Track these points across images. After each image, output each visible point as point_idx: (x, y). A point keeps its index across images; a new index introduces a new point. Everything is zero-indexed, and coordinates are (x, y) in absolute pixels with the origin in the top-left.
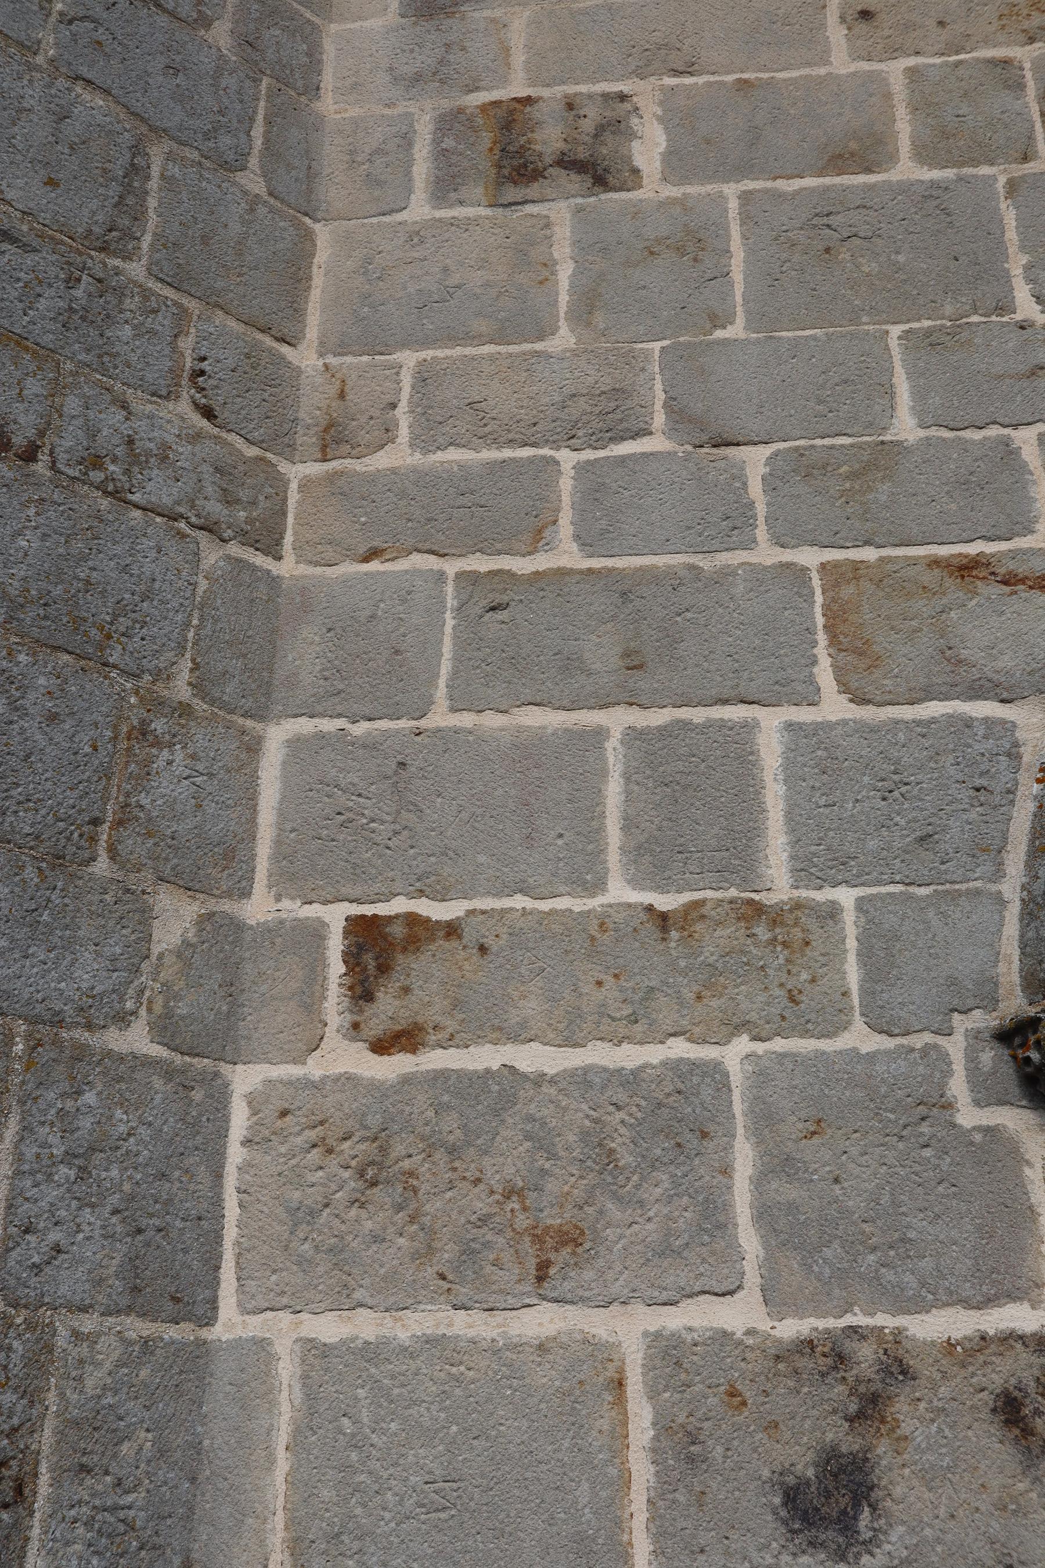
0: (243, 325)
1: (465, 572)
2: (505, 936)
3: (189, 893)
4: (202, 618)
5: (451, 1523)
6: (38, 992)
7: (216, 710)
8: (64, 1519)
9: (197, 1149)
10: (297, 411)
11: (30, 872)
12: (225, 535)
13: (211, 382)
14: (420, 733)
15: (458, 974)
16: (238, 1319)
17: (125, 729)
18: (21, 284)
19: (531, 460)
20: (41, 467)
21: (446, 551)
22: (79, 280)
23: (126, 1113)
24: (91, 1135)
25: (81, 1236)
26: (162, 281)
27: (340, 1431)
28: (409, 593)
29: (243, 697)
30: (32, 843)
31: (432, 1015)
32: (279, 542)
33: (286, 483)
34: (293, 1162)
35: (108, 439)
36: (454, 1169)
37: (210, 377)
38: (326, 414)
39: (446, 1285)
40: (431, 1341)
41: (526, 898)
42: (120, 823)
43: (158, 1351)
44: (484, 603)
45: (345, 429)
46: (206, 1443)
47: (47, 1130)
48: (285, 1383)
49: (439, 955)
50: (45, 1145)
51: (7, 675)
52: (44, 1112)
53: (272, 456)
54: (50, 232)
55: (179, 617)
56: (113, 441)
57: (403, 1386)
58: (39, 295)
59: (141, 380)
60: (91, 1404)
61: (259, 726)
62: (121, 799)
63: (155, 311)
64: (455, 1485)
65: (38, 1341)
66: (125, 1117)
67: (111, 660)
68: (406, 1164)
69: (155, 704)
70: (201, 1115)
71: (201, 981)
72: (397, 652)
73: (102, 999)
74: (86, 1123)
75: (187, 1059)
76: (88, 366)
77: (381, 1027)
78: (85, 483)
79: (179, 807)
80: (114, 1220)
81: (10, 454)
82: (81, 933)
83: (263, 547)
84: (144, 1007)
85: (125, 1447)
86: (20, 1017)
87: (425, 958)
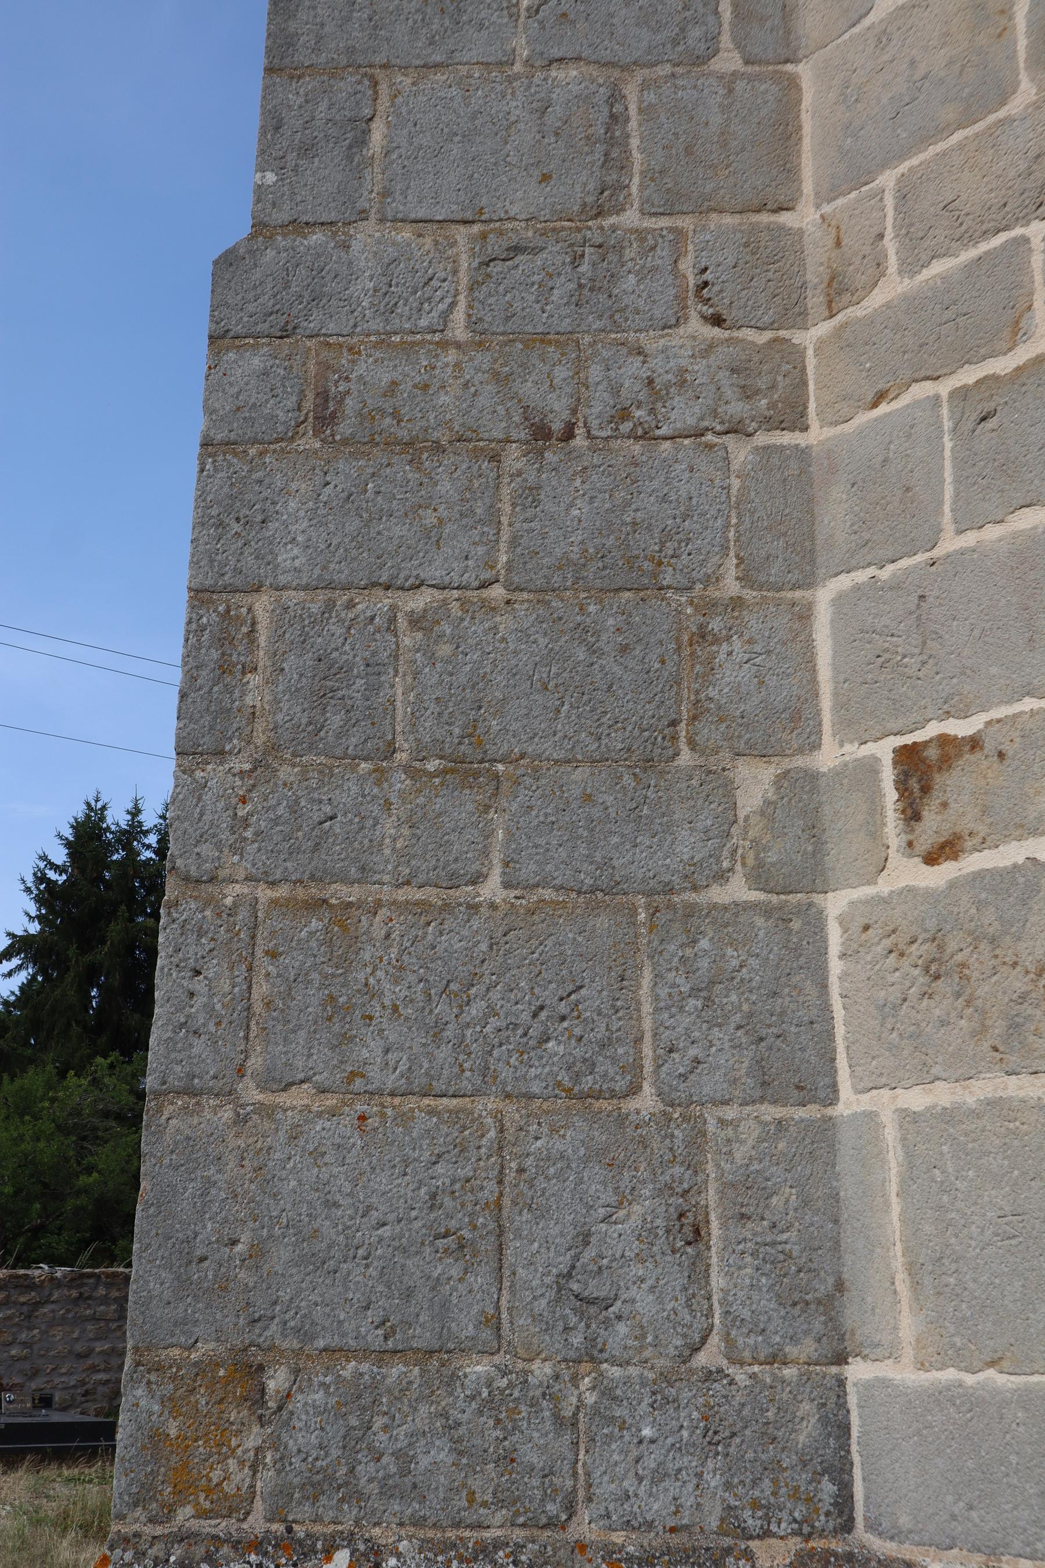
0: (738, 216)
1: (956, 389)
2: (1018, 740)
3: (765, 759)
4: (739, 516)
5: (1020, 1247)
6: (650, 870)
7: (765, 593)
8: (734, 1251)
9: (801, 968)
10: (804, 275)
11: (627, 780)
12: (750, 430)
13: (716, 288)
14: (934, 563)
15: (983, 782)
16: (853, 1097)
17: (687, 638)
18: (536, 287)
19: (1004, 247)
20: (580, 441)
21: (938, 374)
22: (583, 256)
23: (736, 950)
24: (709, 972)
25: (714, 1049)
26: (655, 214)
27: (934, 1180)
28: (912, 427)
29: (789, 572)
30: (625, 756)
31: (968, 823)
32: (803, 414)
33: (802, 352)
34: (877, 967)
35: (631, 387)
36: (996, 956)
37: (713, 284)
38: (828, 268)
39: (998, 1056)
40: (993, 1103)
41: (1034, 700)
42: (695, 718)
43: (791, 1128)
44: (975, 416)
45: (844, 278)
46: (842, 1194)
47: (674, 973)
48: (890, 1144)
49: (967, 768)
50: (674, 985)
51: (582, 627)
52: (670, 961)
53: (785, 332)
54: (552, 225)
55: (719, 522)
56: (635, 389)
57: (974, 1141)
58: (552, 288)
59: (651, 320)
60: (742, 1171)
61: (807, 594)
62: (692, 698)
63: (653, 248)
64: (1020, 1218)
65: (693, 1129)
66: (735, 953)
67: (665, 583)
68: (959, 958)
69: (708, 607)
70: (802, 940)
71: (786, 830)
72: (908, 489)
73: (702, 865)
74: (704, 963)
75: (783, 897)
76: (603, 331)
77: (929, 842)
78: (617, 438)
79: (744, 689)
80: (739, 1033)
81: (554, 441)
82: (676, 817)
83: (788, 424)
84: (739, 863)
85: (774, 1200)
86: (639, 893)
87: (956, 773)
